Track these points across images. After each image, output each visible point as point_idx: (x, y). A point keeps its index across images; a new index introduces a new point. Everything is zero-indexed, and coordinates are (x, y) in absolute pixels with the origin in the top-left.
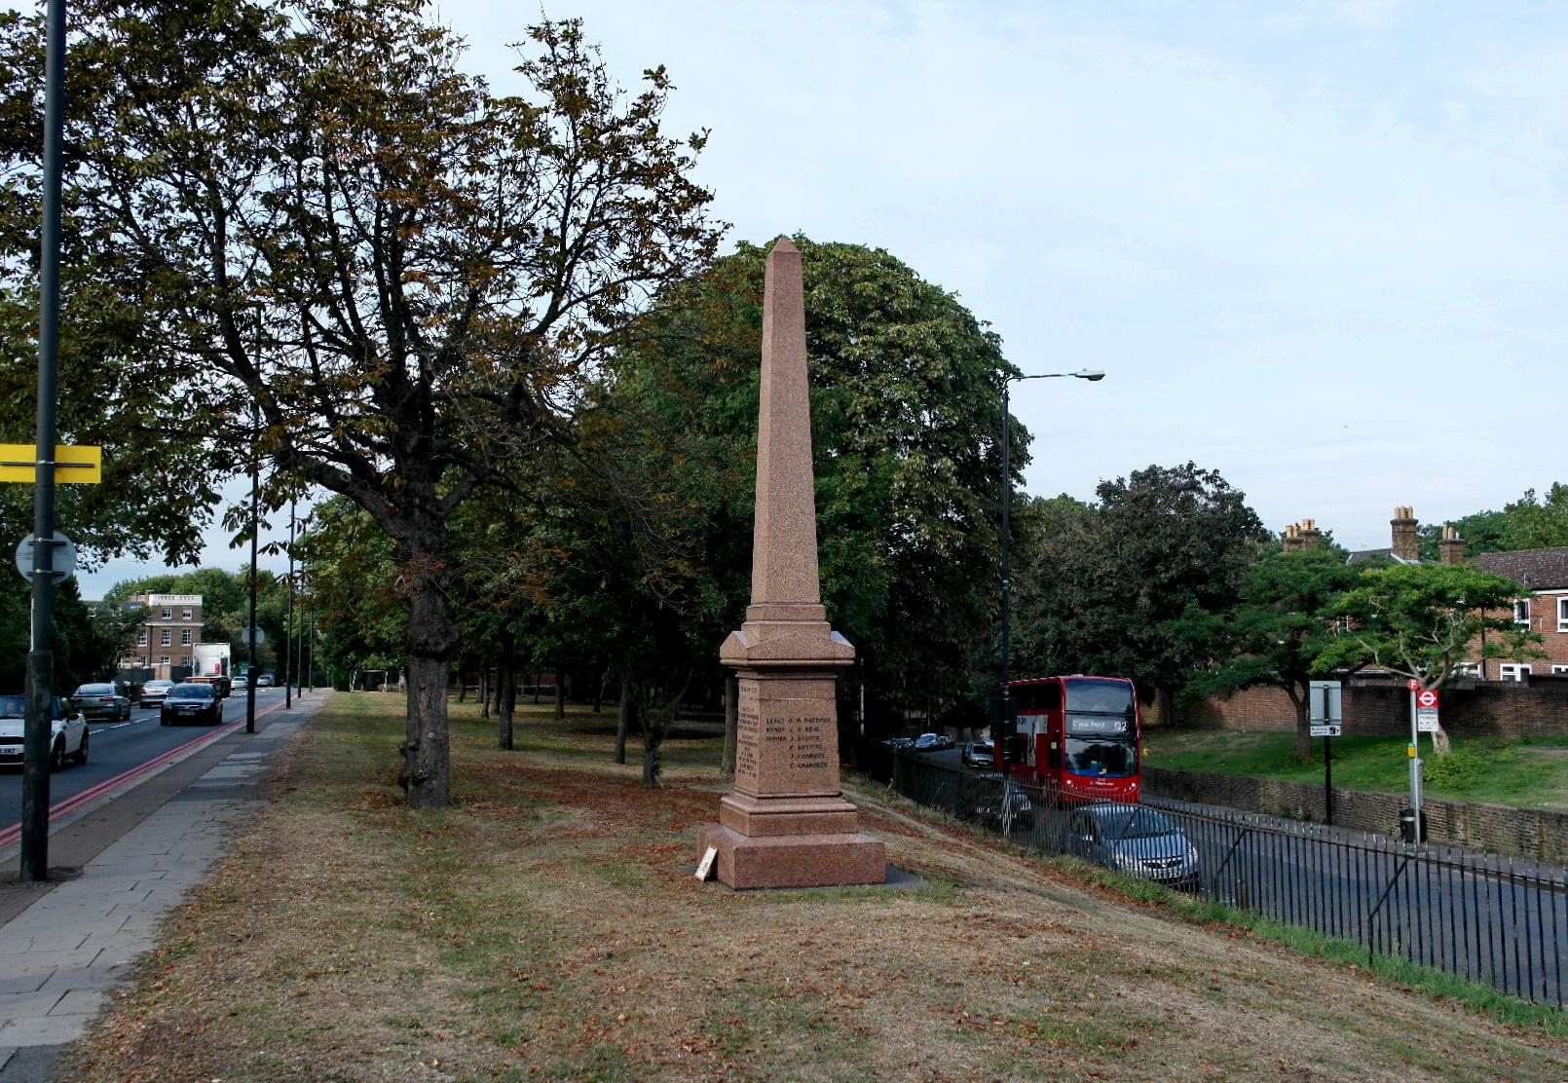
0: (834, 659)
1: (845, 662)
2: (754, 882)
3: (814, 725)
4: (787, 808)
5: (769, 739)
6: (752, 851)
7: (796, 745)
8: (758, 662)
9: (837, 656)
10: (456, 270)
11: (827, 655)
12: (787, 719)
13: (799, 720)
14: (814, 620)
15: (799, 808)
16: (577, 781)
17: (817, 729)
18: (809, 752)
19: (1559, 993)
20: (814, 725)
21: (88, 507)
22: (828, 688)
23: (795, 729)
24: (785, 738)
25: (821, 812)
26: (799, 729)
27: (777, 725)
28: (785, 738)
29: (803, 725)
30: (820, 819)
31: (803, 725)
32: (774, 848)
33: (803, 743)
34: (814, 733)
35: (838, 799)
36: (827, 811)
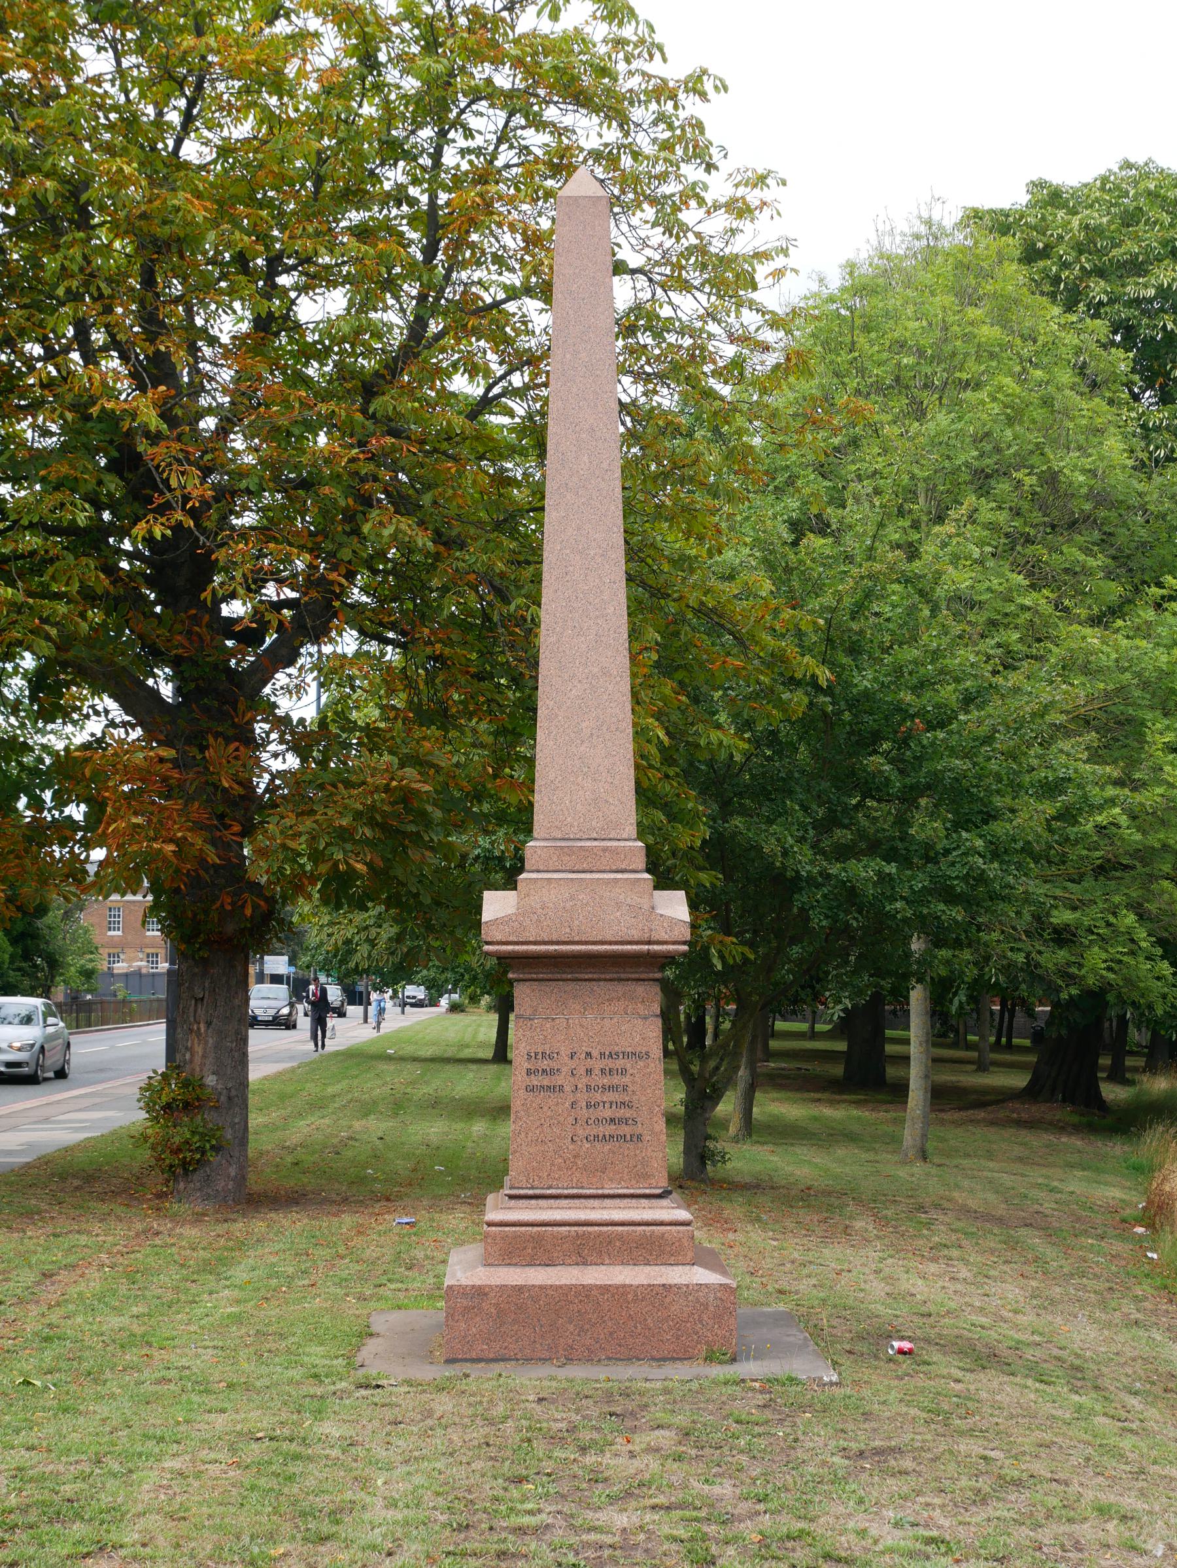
0: (649, 943)
1: (671, 947)
2: (480, 1349)
3: (620, 1063)
4: (558, 1215)
5: (530, 1089)
6: (480, 1292)
7: (582, 1097)
8: (504, 948)
9: (653, 938)
10: (39, 365)
11: (635, 934)
12: (565, 1052)
13: (589, 1054)
14: (622, 871)
15: (582, 1215)
16: (984, 1119)
17: (624, 1072)
18: (608, 1113)
19: (464, 1554)
20: (620, 1063)
21: (825, 344)
22: (649, 999)
23: (582, 1071)
24: (561, 1087)
25: (623, 1224)
26: (589, 1071)
27: (545, 1064)
28: (561, 1087)
29: (598, 1065)
30: (620, 1237)
31: (598, 1065)
32: (520, 1289)
33: (598, 1097)
34: (616, 1080)
35: (664, 1202)
36: (662, 1224)
